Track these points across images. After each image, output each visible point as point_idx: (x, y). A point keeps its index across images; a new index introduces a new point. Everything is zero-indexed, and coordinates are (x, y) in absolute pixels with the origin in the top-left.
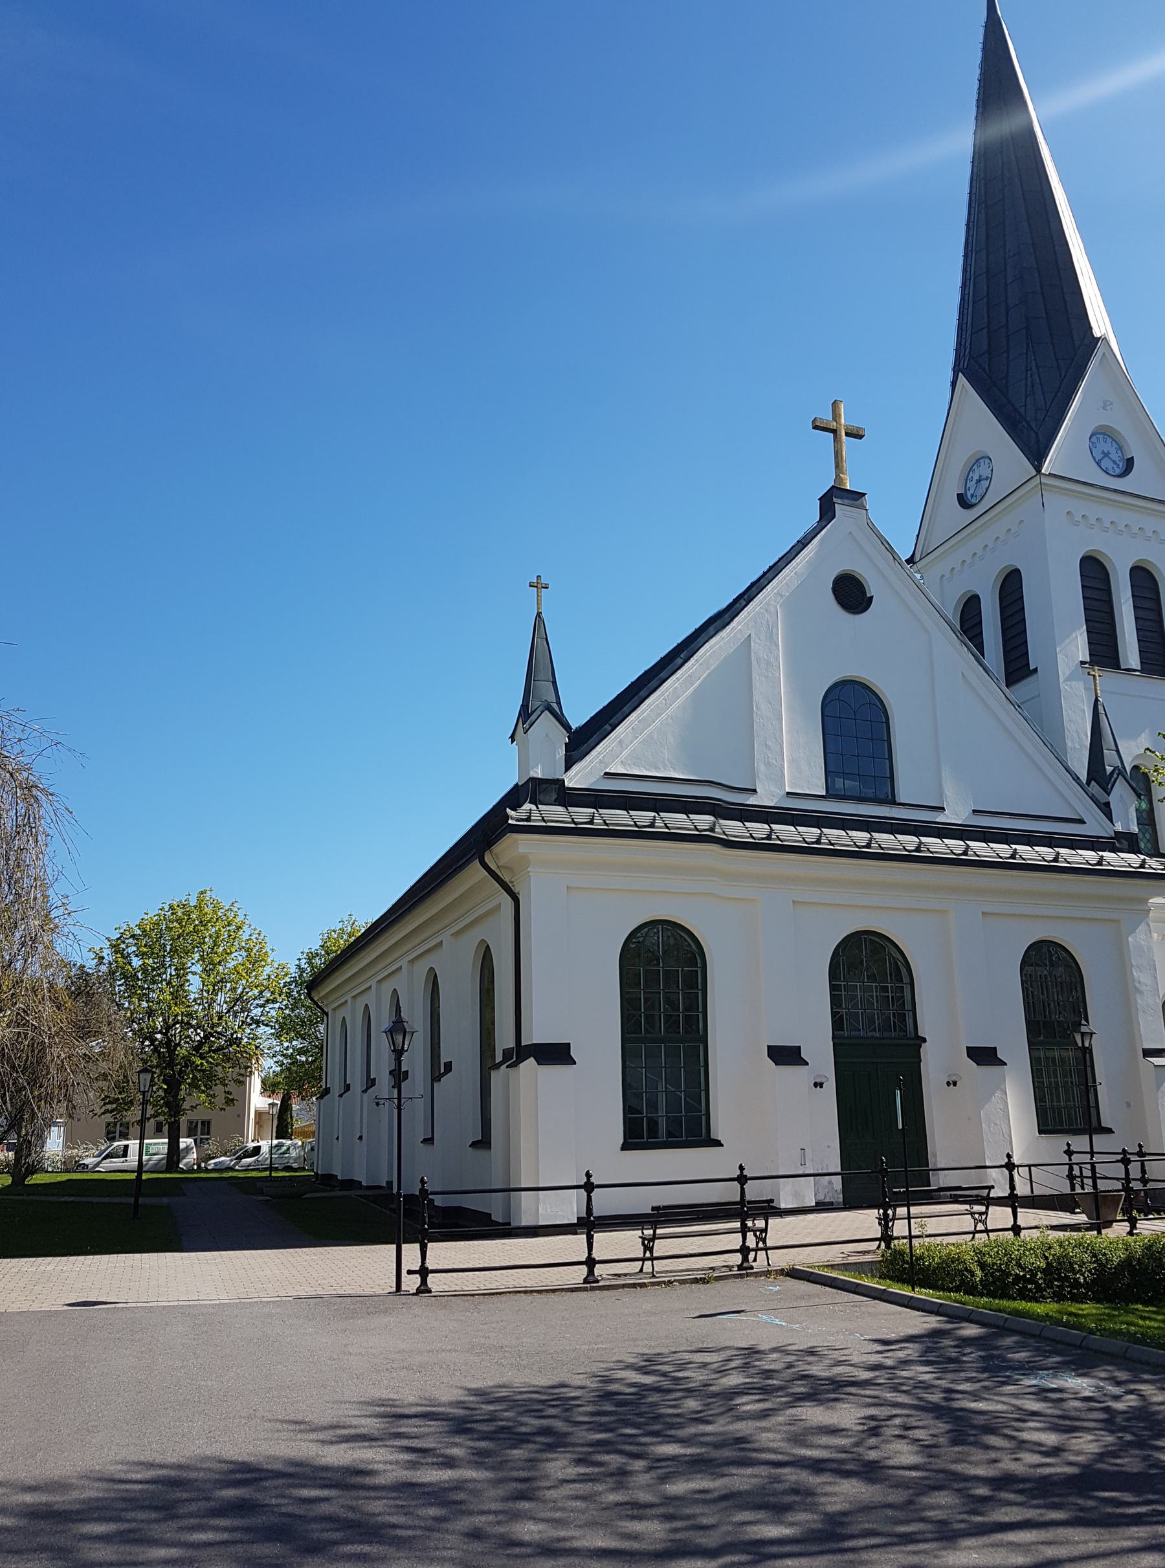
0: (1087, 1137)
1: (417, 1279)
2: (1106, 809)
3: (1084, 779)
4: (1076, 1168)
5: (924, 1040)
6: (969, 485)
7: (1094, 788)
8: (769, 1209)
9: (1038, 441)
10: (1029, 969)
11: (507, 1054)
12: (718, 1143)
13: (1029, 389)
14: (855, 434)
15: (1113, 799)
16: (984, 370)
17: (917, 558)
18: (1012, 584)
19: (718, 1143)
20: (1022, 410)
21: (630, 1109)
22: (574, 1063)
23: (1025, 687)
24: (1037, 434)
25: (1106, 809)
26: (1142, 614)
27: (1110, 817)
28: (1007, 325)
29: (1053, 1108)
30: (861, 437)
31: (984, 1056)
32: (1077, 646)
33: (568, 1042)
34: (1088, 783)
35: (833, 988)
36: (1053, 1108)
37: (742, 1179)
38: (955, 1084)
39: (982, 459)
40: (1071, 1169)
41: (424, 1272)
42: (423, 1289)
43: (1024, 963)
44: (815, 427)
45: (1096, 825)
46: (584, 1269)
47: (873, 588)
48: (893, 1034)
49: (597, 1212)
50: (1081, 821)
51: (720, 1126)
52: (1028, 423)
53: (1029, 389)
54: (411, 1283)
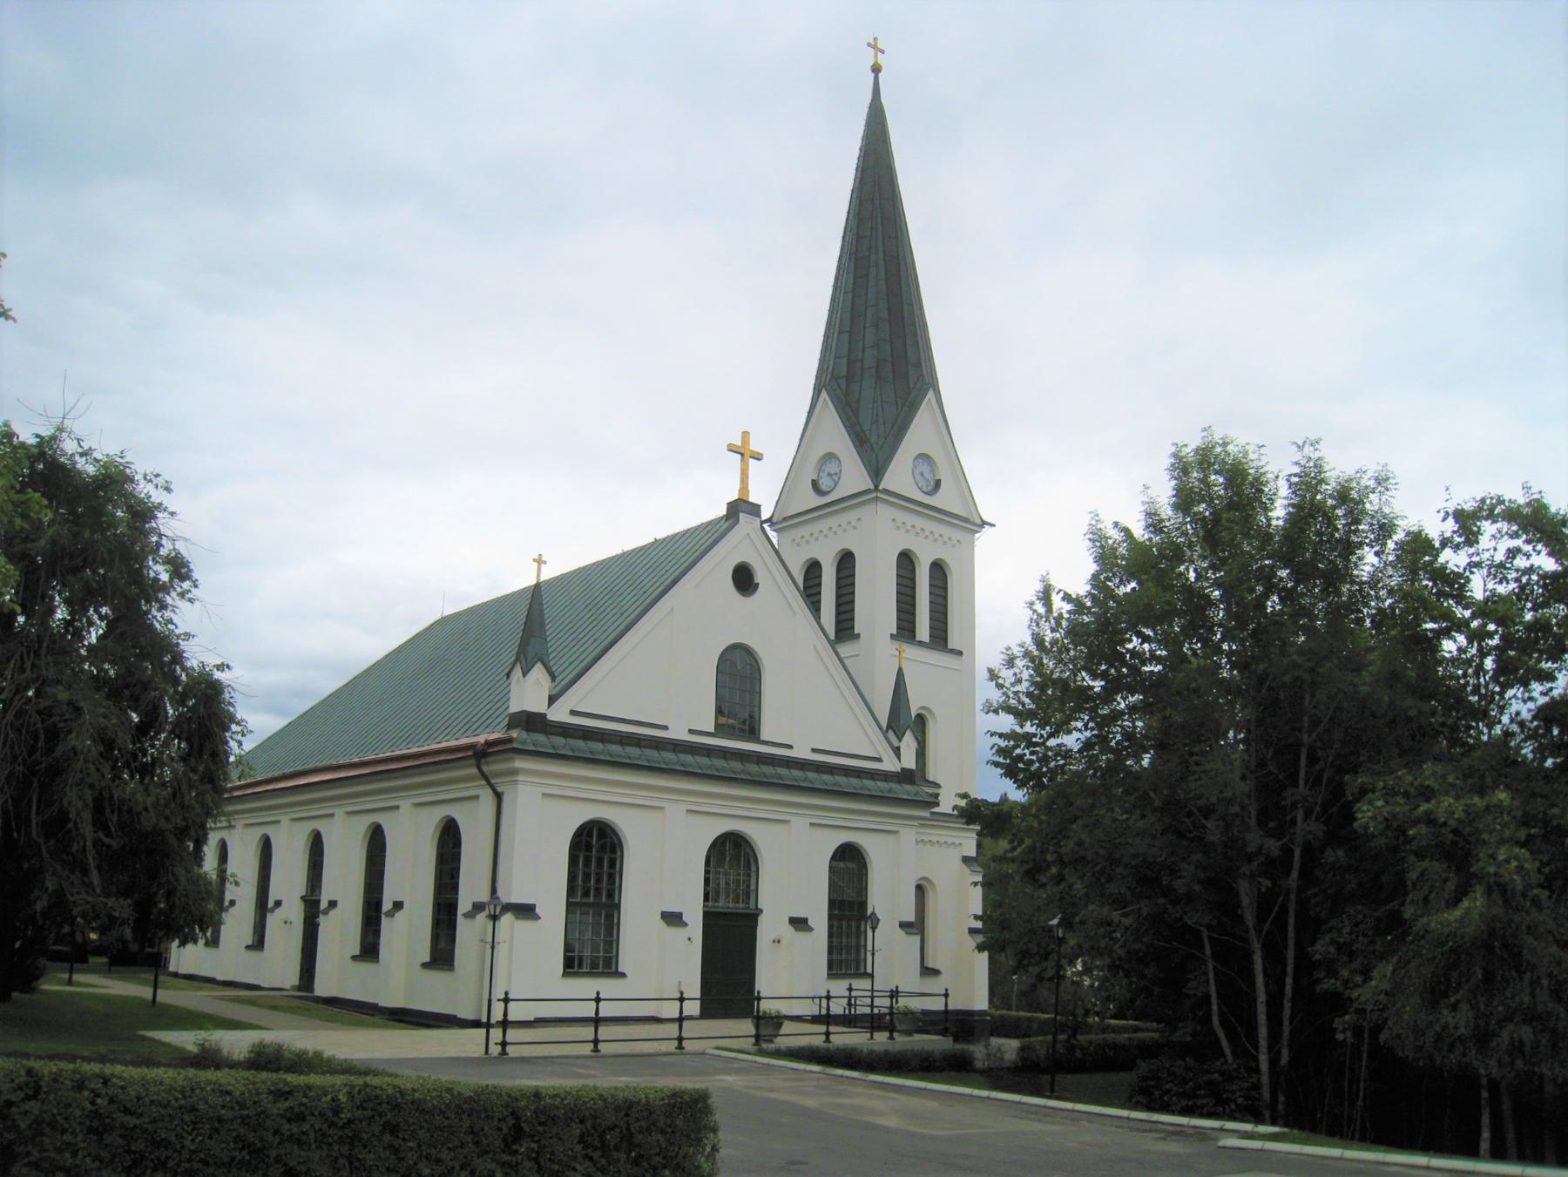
0: (950, 1008)
2: (897, 751)
3: (884, 727)
5: (762, 911)
7: (891, 735)
8: (816, 1020)
9: (878, 462)
10: (835, 863)
11: (478, 907)
12: (623, 975)
14: (758, 457)
15: (903, 745)
16: (841, 390)
17: (774, 520)
18: (846, 561)
19: (623, 975)
20: (868, 433)
23: (846, 650)
24: (877, 456)
25: (897, 751)
28: (862, 361)
30: (759, 459)
31: (799, 923)
37: (598, 1000)
38: (779, 942)
39: (830, 457)
41: (504, 1044)
42: (504, 1052)
43: (833, 858)
44: (920, 889)
45: (890, 764)
46: (591, 1046)
47: (760, 577)
49: (601, 1014)
50: (879, 760)
54: (495, 1050)
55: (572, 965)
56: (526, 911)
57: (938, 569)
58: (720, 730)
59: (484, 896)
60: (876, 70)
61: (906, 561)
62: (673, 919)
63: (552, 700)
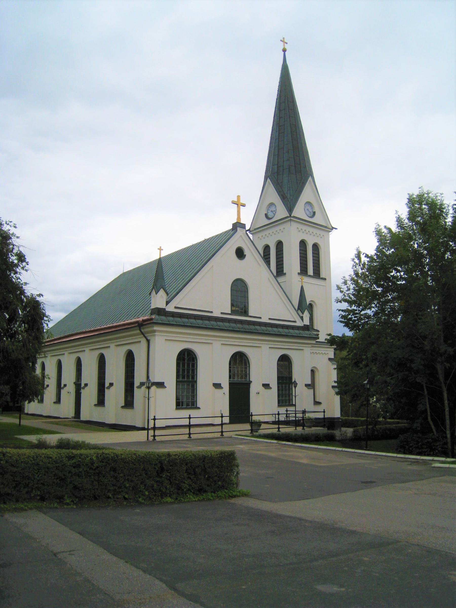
0: (228, 415)
1: (152, 438)
2: (302, 318)
4: (288, 415)
6: (268, 211)
7: (299, 312)
10: (279, 362)
11: (142, 384)
12: (199, 408)
13: (289, 188)
16: (275, 178)
18: (280, 245)
19: (199, 408)
21: (177, 399)
22: (166, 387)
23: (281, 279)
25: (302, 318)
26: (314, 255)
27: (303, 320)
28: (283, 166)
29: (285, 400)
32: (297, 268)
33: (163, 381)
34: (298, 310)
35: (230, 367)
36: (285, 400)
38: (259, 393)
39: (272, 204)
40: (287, 415)
42: (154, 439)
43: (279, 360)
46: (188, 436)
47: (246, 252)
48: (243, 380)
50: (295, 322)
51: (200, 403)
52: (288, 199)
53: (289, 188)
54: (151, 438)
55: (179, 405)
56: (161, 385)
57: (316, 247)
58: (233, 312)
59: (144, 380)
60: (284, 51)
61: (303, 244)
62: (217, 386)
63: (167, 303)
